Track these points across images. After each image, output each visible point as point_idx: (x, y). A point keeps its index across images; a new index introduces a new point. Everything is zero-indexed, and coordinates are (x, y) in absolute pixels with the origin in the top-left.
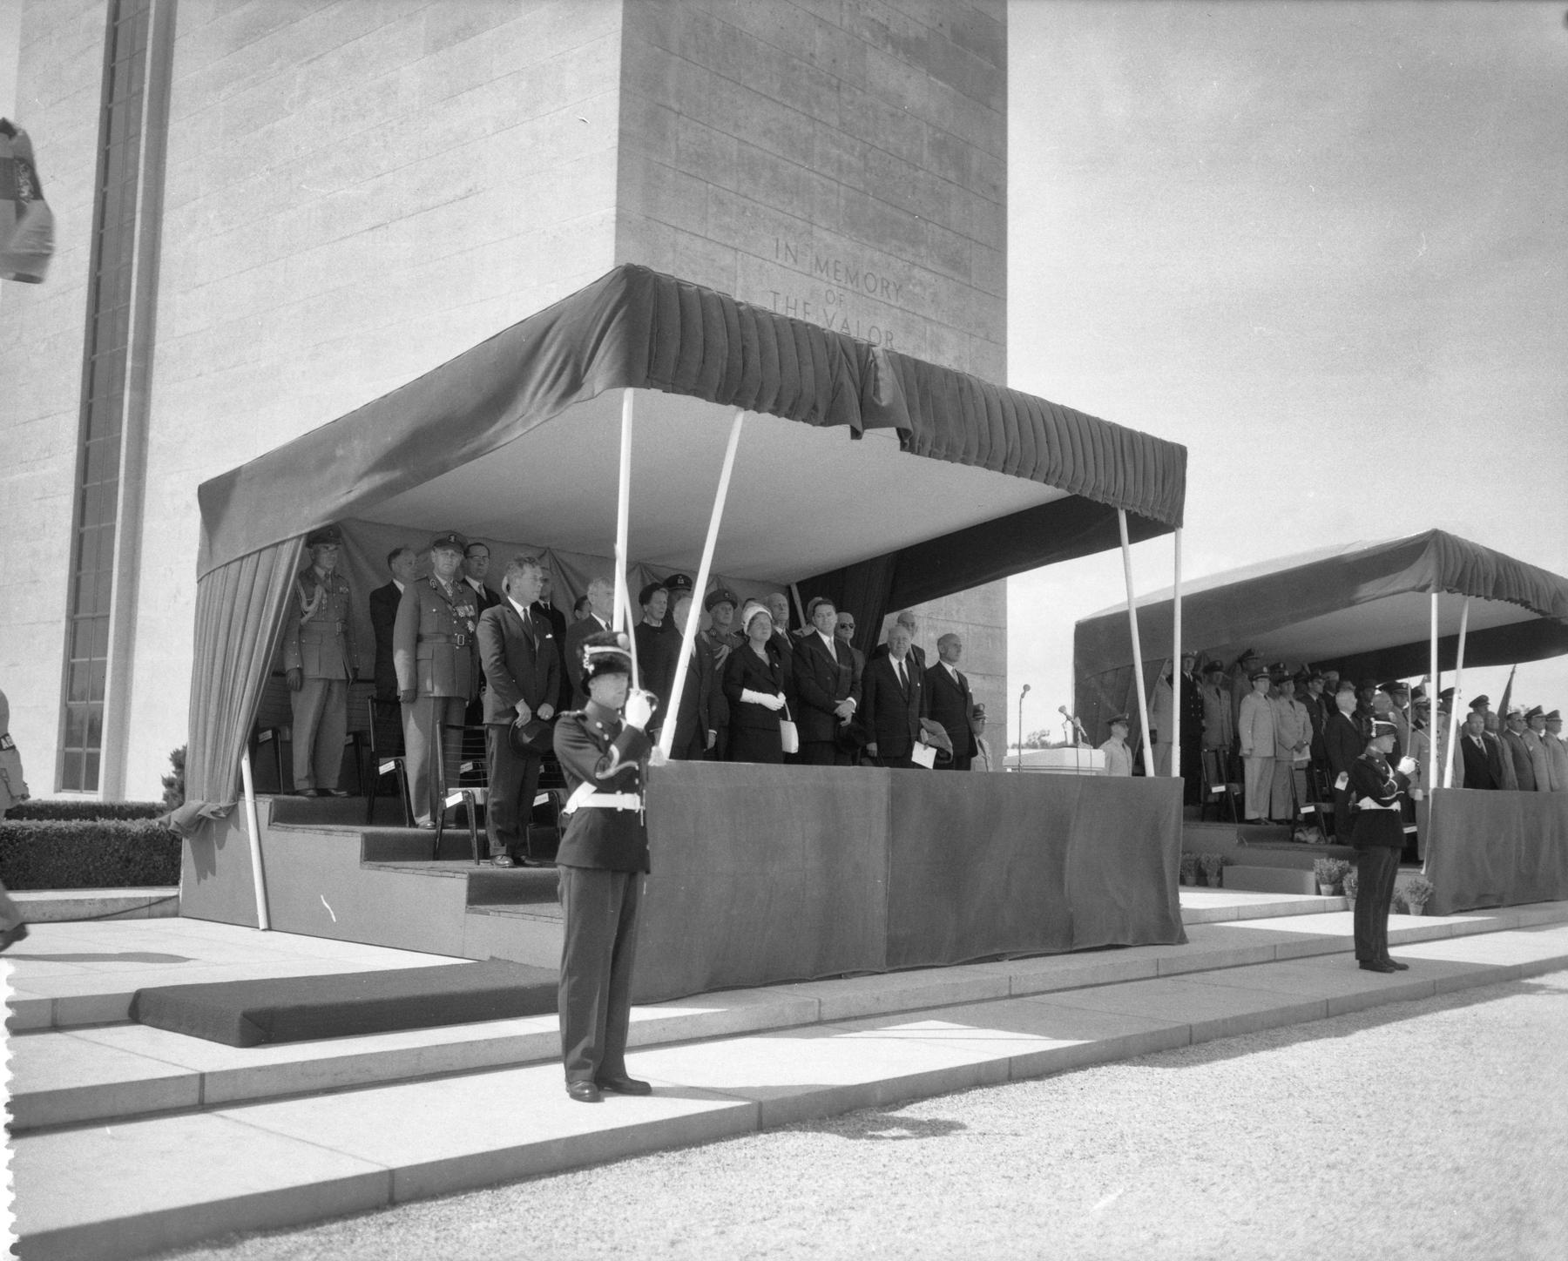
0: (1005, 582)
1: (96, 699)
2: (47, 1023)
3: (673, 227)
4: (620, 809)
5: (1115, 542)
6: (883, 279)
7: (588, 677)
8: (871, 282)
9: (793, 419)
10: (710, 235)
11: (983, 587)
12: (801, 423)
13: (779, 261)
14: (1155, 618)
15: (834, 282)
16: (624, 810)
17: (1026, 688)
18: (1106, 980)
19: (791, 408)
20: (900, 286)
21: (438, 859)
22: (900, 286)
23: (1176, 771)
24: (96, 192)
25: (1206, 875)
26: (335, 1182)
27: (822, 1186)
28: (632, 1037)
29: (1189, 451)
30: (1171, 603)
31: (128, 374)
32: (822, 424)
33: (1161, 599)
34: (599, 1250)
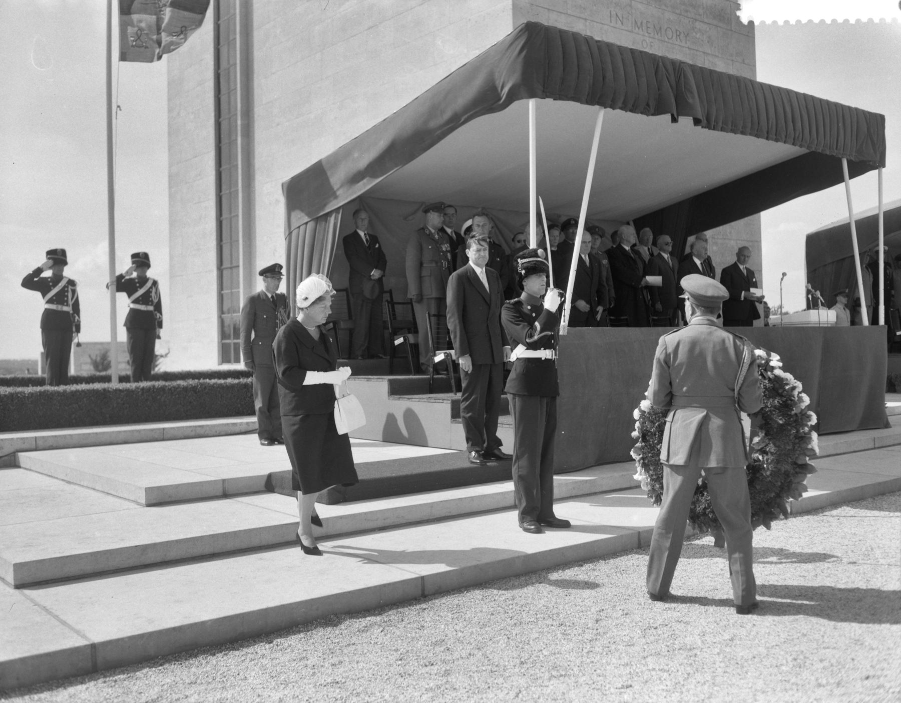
0: (760, 215)
1: (236, 313)
2: (220, 492)
3: (546, 8)
4: (543, 359)
5: (839, 179)
6: (677, 30)
7: (522, 278)
8: (670, 33)
9: (635, 112)
10: (569, 12)
11: (746, 219)
12: (640, 114)
13: (612, 25)
14: (867, 226)
15: (647, 34)
16: (546, 359)
17: (784, 274)
18: (842, 452)
19: (633, 106)
20: (688, 34)
21: (432, 393)
22: (688, 34)
23: (882, 321)
24: (214, 24)
25: (895, 386)
26: (389, 584)
27: (684, 583)
28: (557, 492)
29: (886, 117)
30: (849, 225)
31: (239, 128)
32: (653, 115)
33: (846, 222)
34: (552, 625)
